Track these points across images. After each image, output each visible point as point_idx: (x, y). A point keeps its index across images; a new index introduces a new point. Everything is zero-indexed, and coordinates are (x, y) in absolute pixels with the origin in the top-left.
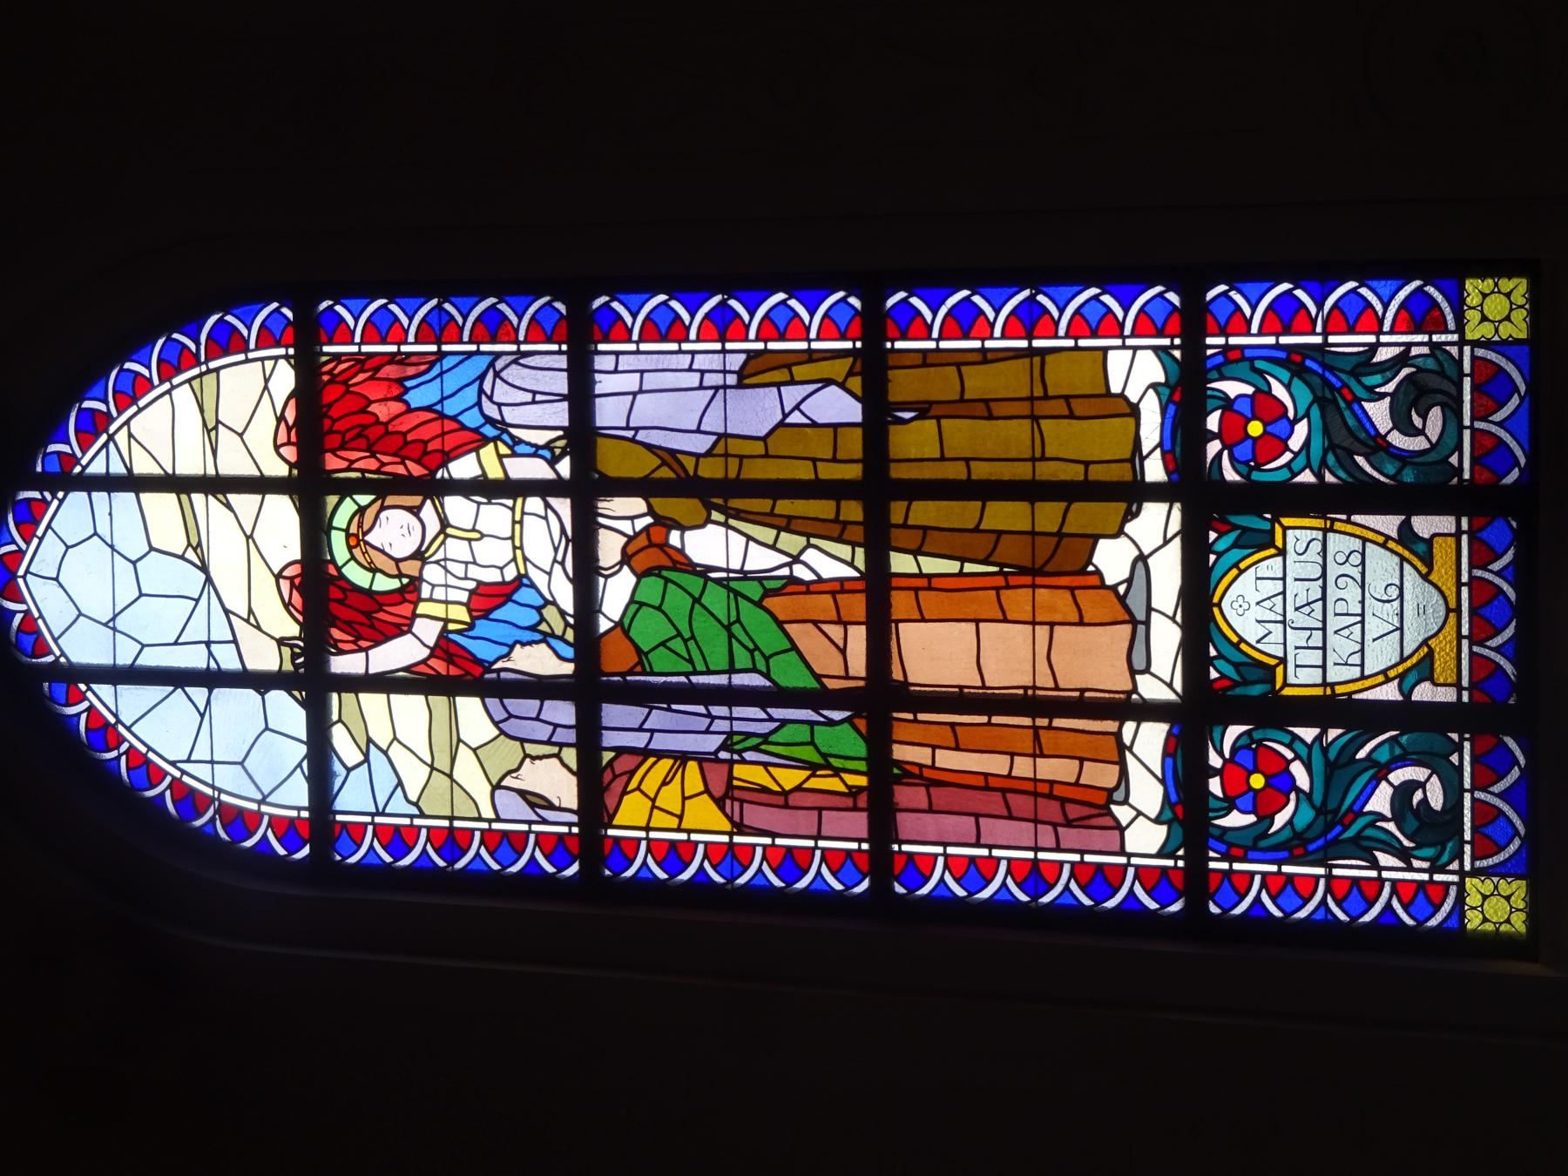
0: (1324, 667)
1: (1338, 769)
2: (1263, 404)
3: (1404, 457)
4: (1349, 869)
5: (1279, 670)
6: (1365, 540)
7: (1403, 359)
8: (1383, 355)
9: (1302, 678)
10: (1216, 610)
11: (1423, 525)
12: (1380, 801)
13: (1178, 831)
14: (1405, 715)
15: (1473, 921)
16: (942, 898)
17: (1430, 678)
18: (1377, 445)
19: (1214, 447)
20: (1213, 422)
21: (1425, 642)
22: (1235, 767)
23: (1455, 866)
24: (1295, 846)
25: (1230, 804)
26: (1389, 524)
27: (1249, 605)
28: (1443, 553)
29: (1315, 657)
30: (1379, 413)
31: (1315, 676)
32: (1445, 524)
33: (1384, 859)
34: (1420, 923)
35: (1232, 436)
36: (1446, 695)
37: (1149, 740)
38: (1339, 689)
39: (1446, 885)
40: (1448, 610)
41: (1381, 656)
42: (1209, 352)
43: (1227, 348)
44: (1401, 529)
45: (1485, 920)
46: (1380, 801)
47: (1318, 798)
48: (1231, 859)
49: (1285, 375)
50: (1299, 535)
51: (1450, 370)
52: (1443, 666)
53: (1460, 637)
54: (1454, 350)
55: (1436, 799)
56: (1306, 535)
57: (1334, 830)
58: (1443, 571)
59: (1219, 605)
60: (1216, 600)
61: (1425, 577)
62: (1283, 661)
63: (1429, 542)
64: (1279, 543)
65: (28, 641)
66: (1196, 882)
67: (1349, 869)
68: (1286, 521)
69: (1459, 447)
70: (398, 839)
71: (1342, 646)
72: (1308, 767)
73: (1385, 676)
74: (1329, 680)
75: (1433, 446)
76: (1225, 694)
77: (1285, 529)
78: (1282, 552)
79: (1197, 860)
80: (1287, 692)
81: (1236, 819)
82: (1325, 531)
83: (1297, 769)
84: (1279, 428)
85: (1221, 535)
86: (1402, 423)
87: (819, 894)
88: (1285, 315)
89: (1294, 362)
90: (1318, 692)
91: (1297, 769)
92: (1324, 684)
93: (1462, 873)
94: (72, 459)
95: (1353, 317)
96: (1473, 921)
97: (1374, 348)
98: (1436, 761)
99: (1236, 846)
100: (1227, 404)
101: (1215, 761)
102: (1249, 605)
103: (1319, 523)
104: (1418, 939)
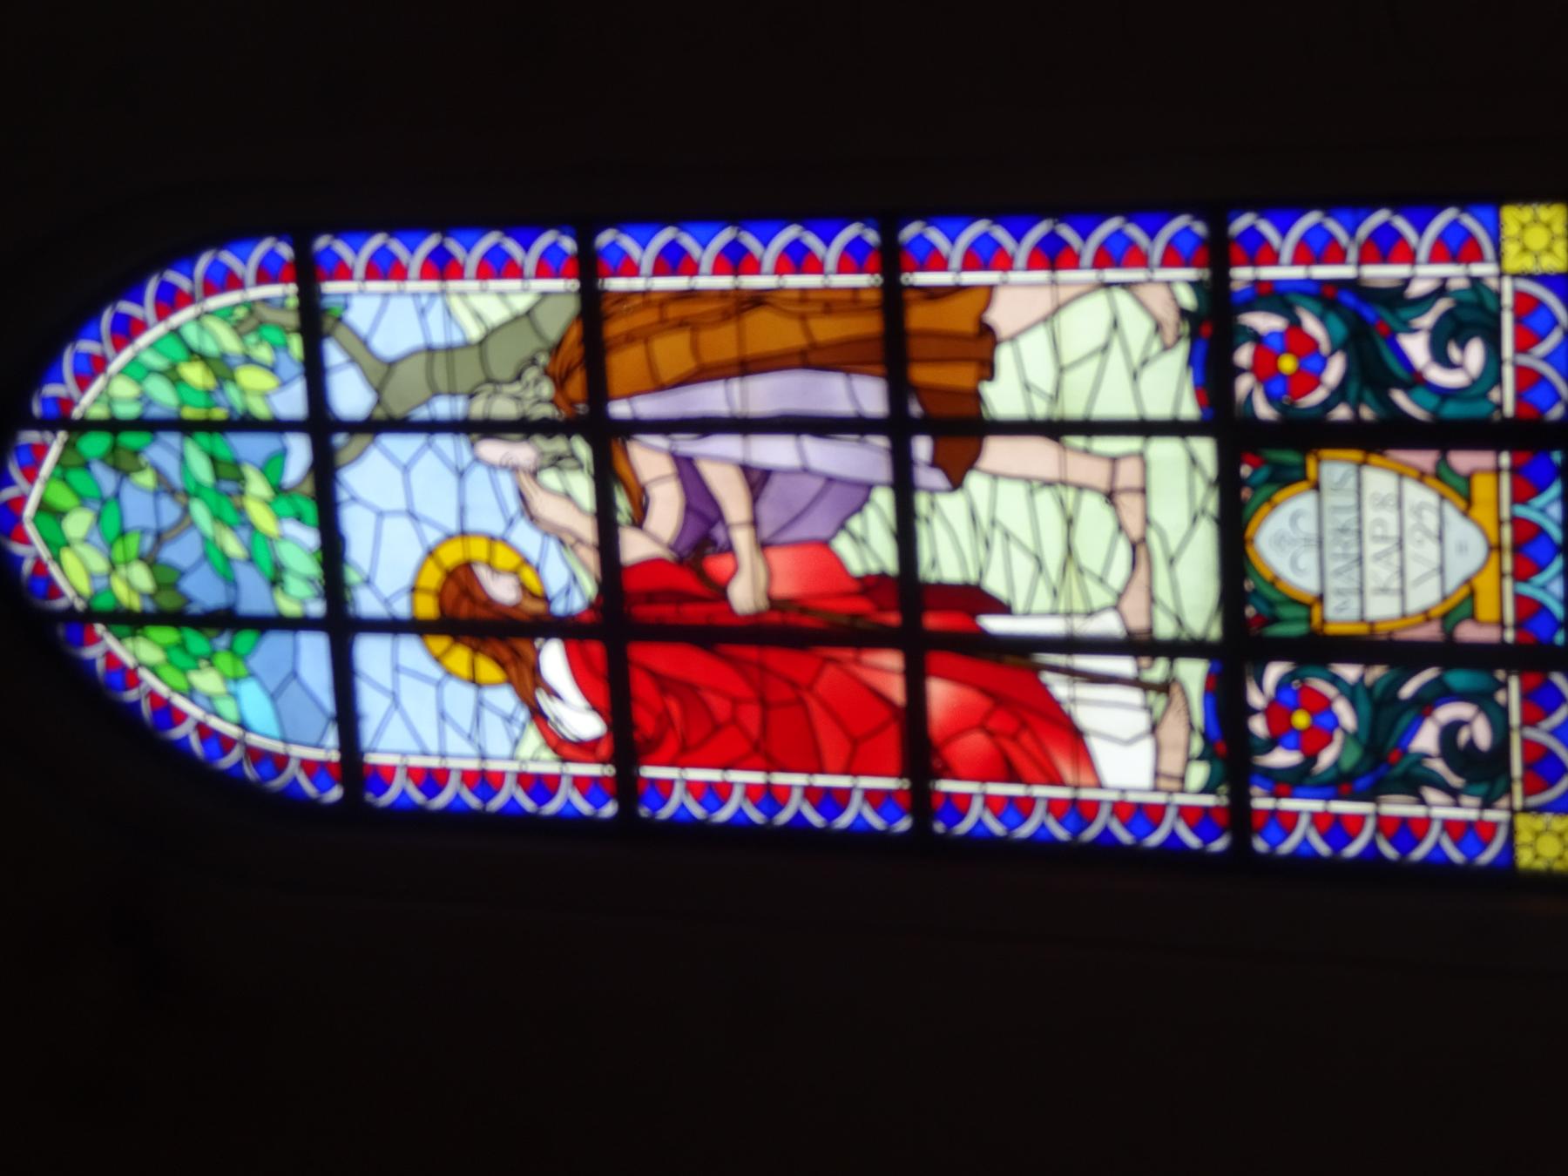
1: (1387, 719)
2: (1295, 339)
3: (1445, 394)
4: (1398, 807)
7: (1441, 291)
8: (1418, 289)
11: (1462, 460)
12: (1426, 739)
13: (1219, 766)
14: (1448, 653)
15: (1525, 858)
16: (980, 837)
17: (1472, 616)
18: (1414, 380)
19: (1244, 384)
20: (1244, 355)
21: (1468, 582)
22: (1278, 712)
23: (1504, 802)
24: (1339, 784)
25: (1272, 743)
26: (1425, 459)
27: (1285, 540)
28: (1483, 488)
30: (1416, 347)
31: (1352, 612)
32: (1483, 459)
33: (1432, 795)
34: (1471, 858)
35: (1265, 370)
36: (1488, 635)
37: (1193, 673)
39: (1493, 826)
41: (1424, 596)
43: (1257, 283)
44: (1437, 465)
45: (1537, 857)
46: (1426, 739)
47: (1364, 737)
48: (1277, 795)
49: (1317, 307)
50: (1335, 469)
51: (1490, 303)
52: (1486, 609)
53: (1502, 575)
55: (1481, 734)
56: (1344, 615)
57: (1383, 766)
58: (1483, 511)
62: (1321, 599)
63: (1468, 478)
65: (40, 586)
66: (1239, 818)
67: (1398, 807)
69: (1498, 381)
70: (432, 780)
71: (1379, 572)
72: (1353, 703)
73: (1426, 616)
75: (1474, 382)
76: (1254, 628)
78: (1316, 487)
79: (1240, 799)
81: (1282, 758)
83: (1343, 710)
84: (1313, 364)
85: (1256, 467)
86: (1440, 356)
87: (860, 831)
88: (1317, 249)
89: (1327, 296)
91: (1343, 710)
93: (1512, 811)
94: (69, 403)
95: (1386, 246)
96: (1525, 858)
97: (1407, 282)
98: (1484, 699)
99: (1284, 782)
100: (1257, 338)
101: (1256, 699)
102: (1285, 540)
104: (1467, 876)
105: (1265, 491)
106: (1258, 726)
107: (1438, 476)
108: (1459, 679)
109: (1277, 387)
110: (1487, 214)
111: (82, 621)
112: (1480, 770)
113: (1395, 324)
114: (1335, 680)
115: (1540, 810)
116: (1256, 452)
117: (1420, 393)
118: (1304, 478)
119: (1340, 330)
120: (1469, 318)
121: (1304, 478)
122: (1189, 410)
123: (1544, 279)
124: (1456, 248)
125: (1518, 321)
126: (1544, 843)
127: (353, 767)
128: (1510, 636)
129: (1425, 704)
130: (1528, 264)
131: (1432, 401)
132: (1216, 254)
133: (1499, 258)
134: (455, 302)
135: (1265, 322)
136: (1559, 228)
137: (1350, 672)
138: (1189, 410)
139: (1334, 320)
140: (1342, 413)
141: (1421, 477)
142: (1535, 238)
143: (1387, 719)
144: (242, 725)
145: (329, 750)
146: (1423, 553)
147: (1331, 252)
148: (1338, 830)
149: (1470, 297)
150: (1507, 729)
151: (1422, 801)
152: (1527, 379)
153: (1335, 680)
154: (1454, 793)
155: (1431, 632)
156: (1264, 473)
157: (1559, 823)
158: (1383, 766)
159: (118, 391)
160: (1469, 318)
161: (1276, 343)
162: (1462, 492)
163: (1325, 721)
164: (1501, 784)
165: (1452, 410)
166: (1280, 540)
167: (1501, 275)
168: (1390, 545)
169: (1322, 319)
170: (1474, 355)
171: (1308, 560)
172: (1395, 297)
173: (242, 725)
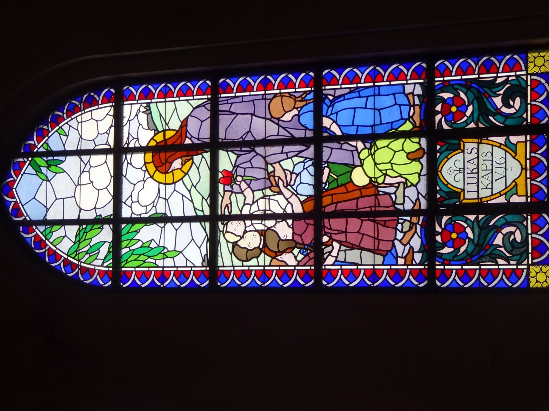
0: (478, 191)
3: (507, 116)
5: (462, 194)
6: (493, 146)
8: (499, 80)
9: (470, 196)
10: (439, 173)
11: (514, 139)
12: (498, 241)
15: (533, 284)
18: (498, 112)
20: (438, 108)
21: (514, 181)
22: (445, 232)
23: (526, 262)
24: (468, 259)
26: (501, 140)
27: (454, 171)
28: (521, 149)
29: (474, 188)
30: (498, 101)
31: (475, 195)
32: (522, 138)
33: (500, 261)
35: (445, 112)
38: (483, 200)
40: (522, 169)
41: (499, 186)
42: (437, 84)
46: (498, 241)
48: (444, 265)
50: (470, 145)
51: (523, 84)
52: (521, 190)
54: (524, 77)
59: (441, 171)
60: (439, 170)
61: (514, 157)
62: (463, 190)
64: (462, 148)
68: (465, 140)
73: (500, 194)
74: (480, 197)
75: (517, 111)
76: (441, 203)
77: (464, 199)
78: (463, 151)
79: (432, 266)
80: (465, 201)
81: (446, 250)
82: (479, 143)
89: (467, 85)
90: (476, 201)
92: (478, 198)
93: (528, 265)
95: (488, 67)
96: (533, 284)
100: (443, 101)
102: (454, 171)
103: (476, 140)
105: (446, 153)
106: (438, 238)
107: (505, 145)
108: (509, 218)
109: (450, 117)
110: (523, 56)
111: (29, 225)
112: (517, 250)
113: (491, 94)
114: (466, 220)
115: (538, 264)
116: (438, 141)
117: (498, 117)
118: (460, 148)
119: (472, 97)
120: (515, 90)
121: (460, 148)
122: (358, 133)
123: (541, 75)
124: (512, 66)
125: (532, 90)
126: (541, 277)
127: (117, 273)
128: (529, 200)
129: (498, 229)
130: (536, 70)
131: (502, 119)
132: (428, 75)
133: (527, 69)
134: (153, 106)
135: (446, 95)
136: (536, 54)
137: (472, 217)
138: (358, 133)
139: (469, 93)
140: (472, 125)
141: (500, 146)
142: (541, 62)
143: (486, 231)
144: (401, 176)
145: (108, 266)
146: (499, 172)
147: (468, 70)
148: (466, 276)
149: (516, 83)
150: (527, 234)
151: (497, 264)
152: (536, 110)
153: (466, 220)
154: (507, 259)
155: (502, 200)
156: (444, 148)
157: (544, 269)
158: (483, 250)
159: (54, 142)
160: (515, 90)
161: (450, 102)
162: (512, 149)
163: (462, 236)
164: (524, 256)
165: (509, 122)
166: (450, 172)
167: (527, 75)
168: (488, 170)
169: (466, 94)
170: (518, 102)
171: (460, 177)
172: (492, 84)
173: (401, 176)
